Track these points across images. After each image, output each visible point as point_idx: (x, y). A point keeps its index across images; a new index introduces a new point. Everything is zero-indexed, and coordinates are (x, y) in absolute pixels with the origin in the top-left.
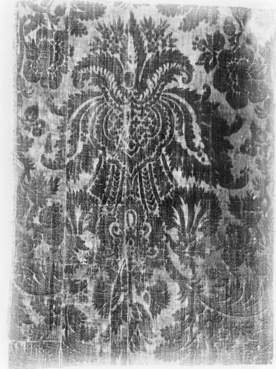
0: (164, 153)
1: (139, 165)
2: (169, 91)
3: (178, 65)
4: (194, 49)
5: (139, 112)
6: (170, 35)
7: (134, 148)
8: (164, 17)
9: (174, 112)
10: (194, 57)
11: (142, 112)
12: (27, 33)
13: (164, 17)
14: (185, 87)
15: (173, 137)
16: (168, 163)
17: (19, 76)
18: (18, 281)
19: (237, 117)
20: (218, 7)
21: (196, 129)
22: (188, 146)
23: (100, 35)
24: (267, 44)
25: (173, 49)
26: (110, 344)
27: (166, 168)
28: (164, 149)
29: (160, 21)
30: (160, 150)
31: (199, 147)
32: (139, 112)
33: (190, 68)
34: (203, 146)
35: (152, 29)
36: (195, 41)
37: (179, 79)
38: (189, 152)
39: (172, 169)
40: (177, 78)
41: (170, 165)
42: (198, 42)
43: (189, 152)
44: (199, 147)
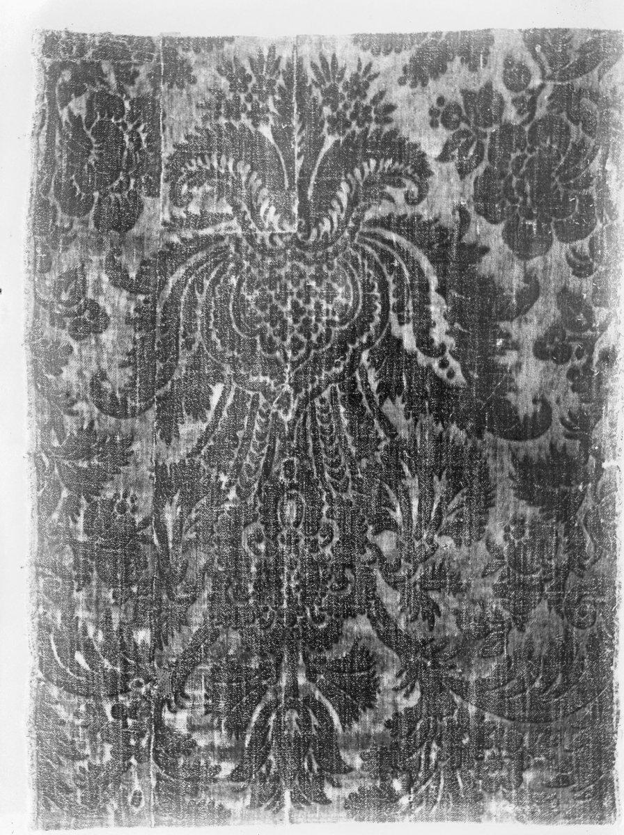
0: (367, 364)
1: (310, 389)
2: (374, 223)
3: (397, 164)
4: (433, 124)
5: (312, 270)
6: (382, 94)
7: (302, 352)
8: (366, 57)
9: (394, 295)
10: (431, 143)
11: (319, 270)
12: (65, 103)
13: (366, 57)
14: (409, 211)
15: (388, 325)
16: (374, 386)
17: (45, 204)
18: (45, 665)
19: (528, 277)
20: (489, 30)
21: (437, 308)
22: (419, 344)
23: (224, 83)
24: (538, 400)
25: (387, 128)
26: (217, 776)
27: (370, 397)
28: (365, 355)
29: (356, 63)
30: (356, 356)
31: (443, 346)
32: (312, 270)
33: (422, 170)
34: (451, 342)
35: (339, 80)
36: (435, 106)
37: (399, 195)
38: (422, 359)
39: (382, 399)
40: (393, 194)
41: (378, 391)
42: (442, 109)
43: (422, 359)
44: (443, 346)
